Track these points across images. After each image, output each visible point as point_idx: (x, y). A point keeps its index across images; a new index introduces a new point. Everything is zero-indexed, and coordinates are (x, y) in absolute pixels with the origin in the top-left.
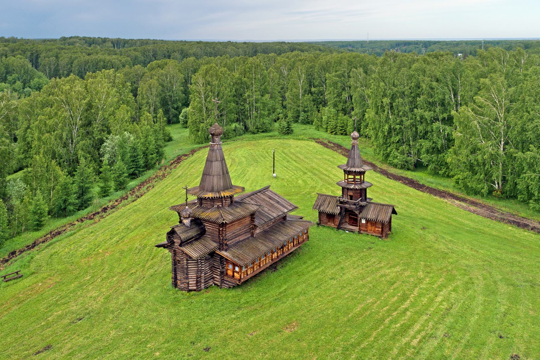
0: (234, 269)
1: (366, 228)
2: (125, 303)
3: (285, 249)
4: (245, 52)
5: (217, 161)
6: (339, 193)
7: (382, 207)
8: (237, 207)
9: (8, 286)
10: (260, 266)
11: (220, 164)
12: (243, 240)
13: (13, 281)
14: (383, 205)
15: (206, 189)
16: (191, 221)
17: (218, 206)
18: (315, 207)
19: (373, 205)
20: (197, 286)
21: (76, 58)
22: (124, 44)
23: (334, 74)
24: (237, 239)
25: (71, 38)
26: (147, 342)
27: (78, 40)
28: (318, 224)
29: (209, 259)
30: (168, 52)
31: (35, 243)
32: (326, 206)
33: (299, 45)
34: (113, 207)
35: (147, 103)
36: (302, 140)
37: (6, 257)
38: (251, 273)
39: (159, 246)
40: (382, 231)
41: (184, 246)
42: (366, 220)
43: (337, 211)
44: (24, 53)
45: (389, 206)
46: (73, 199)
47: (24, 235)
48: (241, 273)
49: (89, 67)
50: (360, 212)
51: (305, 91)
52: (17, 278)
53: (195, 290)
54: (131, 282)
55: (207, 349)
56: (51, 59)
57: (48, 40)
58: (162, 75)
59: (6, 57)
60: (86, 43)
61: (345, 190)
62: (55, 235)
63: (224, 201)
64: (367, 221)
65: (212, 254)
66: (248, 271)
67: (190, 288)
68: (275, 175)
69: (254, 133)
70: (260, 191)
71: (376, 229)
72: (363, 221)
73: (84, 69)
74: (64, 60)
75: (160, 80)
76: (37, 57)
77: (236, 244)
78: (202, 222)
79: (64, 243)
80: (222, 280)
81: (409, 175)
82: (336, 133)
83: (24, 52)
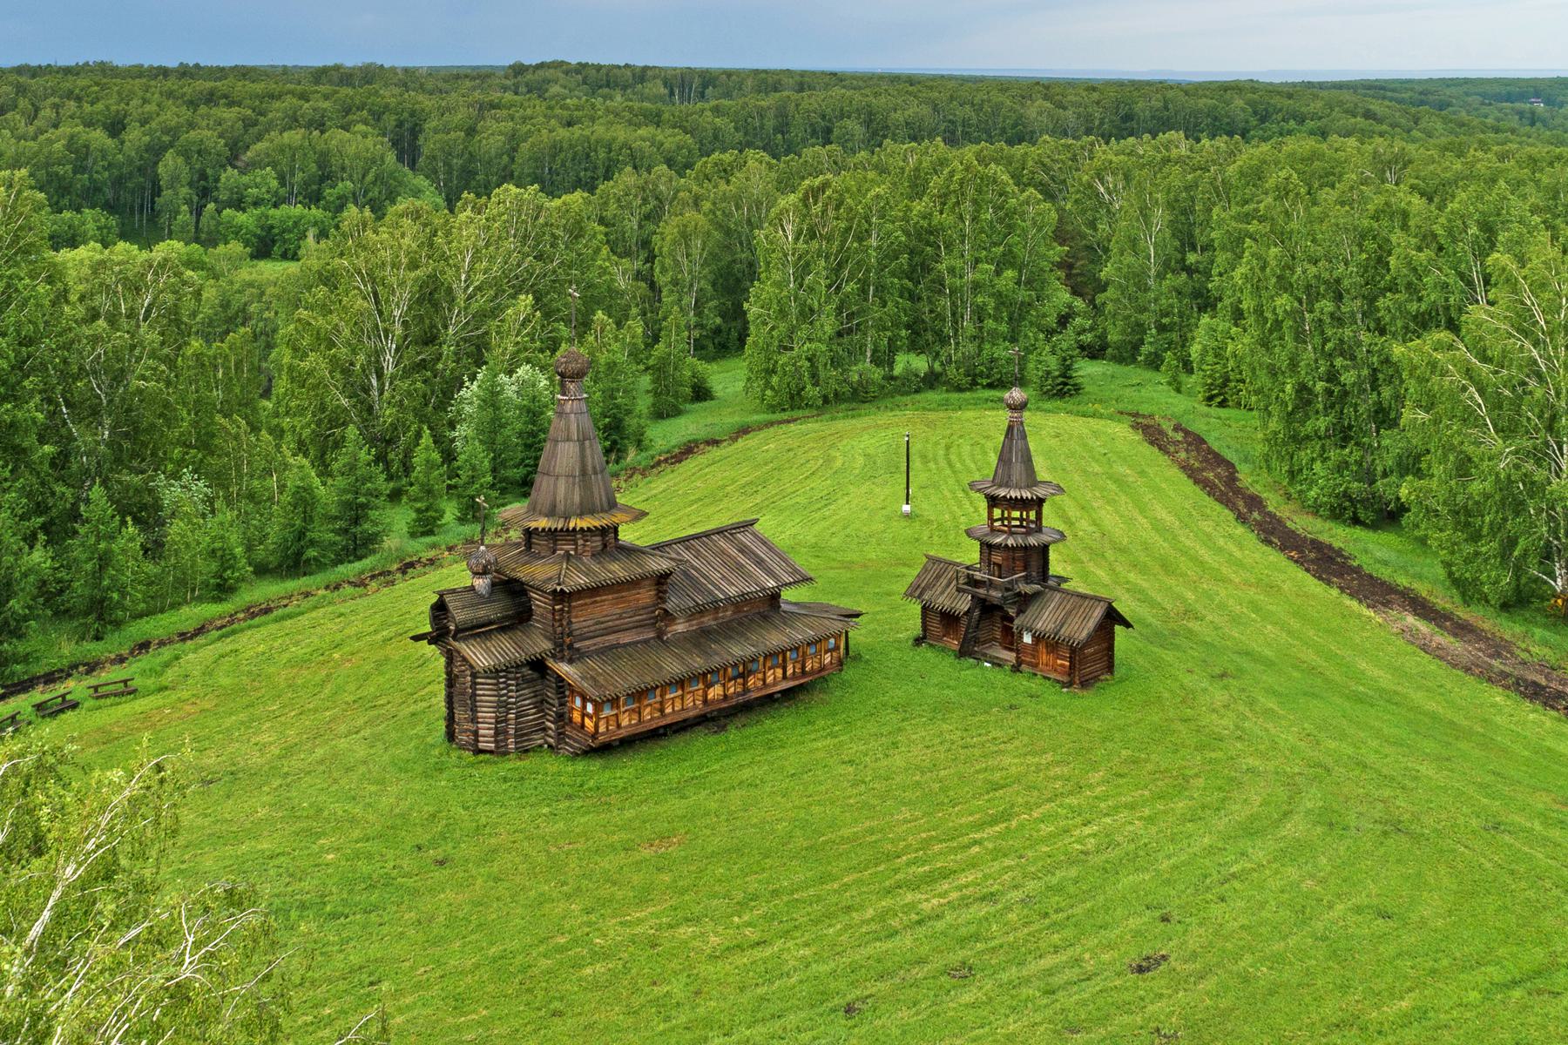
0: (584, 707)
1: (1034, 657)
2: (322, 762)
3: (751, 682)
4: (1089, 118)
5: (568, 439)
6: (970, 554)
7: (1077, 599)
8: (615, 559)
9: (100, 708)
10: (662, 710)
11: (577, 449)
12: (629, 644)
13: (112, 700)
14: (1084, 597)
15: (538, 508)
16: (493, 585)
17: (567, 552)
18: (915, 591)
19: (1059, 595)
20: (496, 742)
21: (529, 134)
22: (705, 86)
23: (1235, 210)
24: (612, 638)
25: (542, 66)
26: (319, 836)
27: (561, 75)
28: (918, 641)
29: (533, 680)
30: (823, 117)
31: (203, 627)
32: (940, 590)
33: (1290, 96)
34: (432, 562)
35: (675, 282)
36: (1093, 416)
37: (125, 652)
38: (630, 725)
39: (416, 638)
40: (1072, 666)
41: (465, 639)
42: (1033, 636)
43: (963, 604)
44: (378, 120)
45: (1099, 600)
46: (324, 533)
47: (185, 610)
48: (599, 719)
49: (563, 165)
50: (1020, 612)
51: (1166, 265)
52: (122, 694)
53: (491, 752)
54: (360, 722)
55: (441, 863)
56: (453, 135)
57: (466, 76)
58: (724, 198)
59: (322, 132)
60: (584, 83)
61: (987, 548)
62: (253, 615)
63: (580, 542)
64: (1038, 639)
65: (538, 666)
66: (621, 717)
67: (481, 745)
68: (906, 508)
69: (959, 389)
70: (720, 532)
71: (1059, 662)
72: (1027, 639)
73: (550, 169)
74: (492, 138)
75: (718, 213)
76: (415, 131)
77: (602, 652)
78: (526, 590)
79: (264, 631)
80: (560, 734)
81: (1338, 536)
82: (1225, 400)
83: (377, 116)
